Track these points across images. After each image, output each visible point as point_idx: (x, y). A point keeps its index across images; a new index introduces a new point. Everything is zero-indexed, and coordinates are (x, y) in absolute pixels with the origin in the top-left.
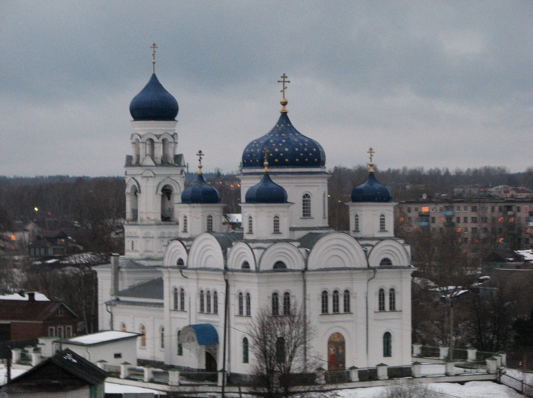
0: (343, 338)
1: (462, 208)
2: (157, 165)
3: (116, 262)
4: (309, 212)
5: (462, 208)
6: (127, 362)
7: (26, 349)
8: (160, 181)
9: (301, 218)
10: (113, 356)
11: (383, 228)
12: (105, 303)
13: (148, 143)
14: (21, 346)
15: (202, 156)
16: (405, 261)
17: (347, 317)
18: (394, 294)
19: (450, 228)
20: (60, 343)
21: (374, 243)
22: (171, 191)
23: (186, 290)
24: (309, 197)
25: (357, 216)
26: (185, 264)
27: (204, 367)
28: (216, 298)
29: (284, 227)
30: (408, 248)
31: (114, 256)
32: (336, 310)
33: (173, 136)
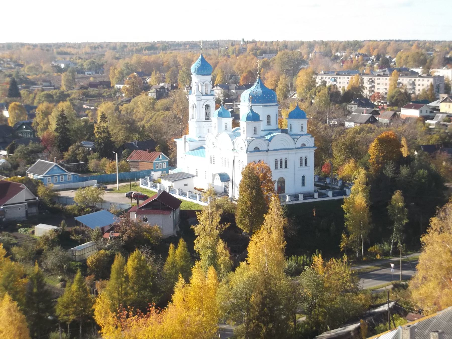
1: (338, 78)
2: (203, 95)
3: (185, 139)
4: (270, 123)
5: (338, 78)
8: (204, 102)
10: (188, 185)
14: (143, 177)
17: (286, 170)
18: (307, 159)
19: (330, 273)
21: (299, 137)
24: (270, 116)
29: (260, 133)
32: (281, 167)
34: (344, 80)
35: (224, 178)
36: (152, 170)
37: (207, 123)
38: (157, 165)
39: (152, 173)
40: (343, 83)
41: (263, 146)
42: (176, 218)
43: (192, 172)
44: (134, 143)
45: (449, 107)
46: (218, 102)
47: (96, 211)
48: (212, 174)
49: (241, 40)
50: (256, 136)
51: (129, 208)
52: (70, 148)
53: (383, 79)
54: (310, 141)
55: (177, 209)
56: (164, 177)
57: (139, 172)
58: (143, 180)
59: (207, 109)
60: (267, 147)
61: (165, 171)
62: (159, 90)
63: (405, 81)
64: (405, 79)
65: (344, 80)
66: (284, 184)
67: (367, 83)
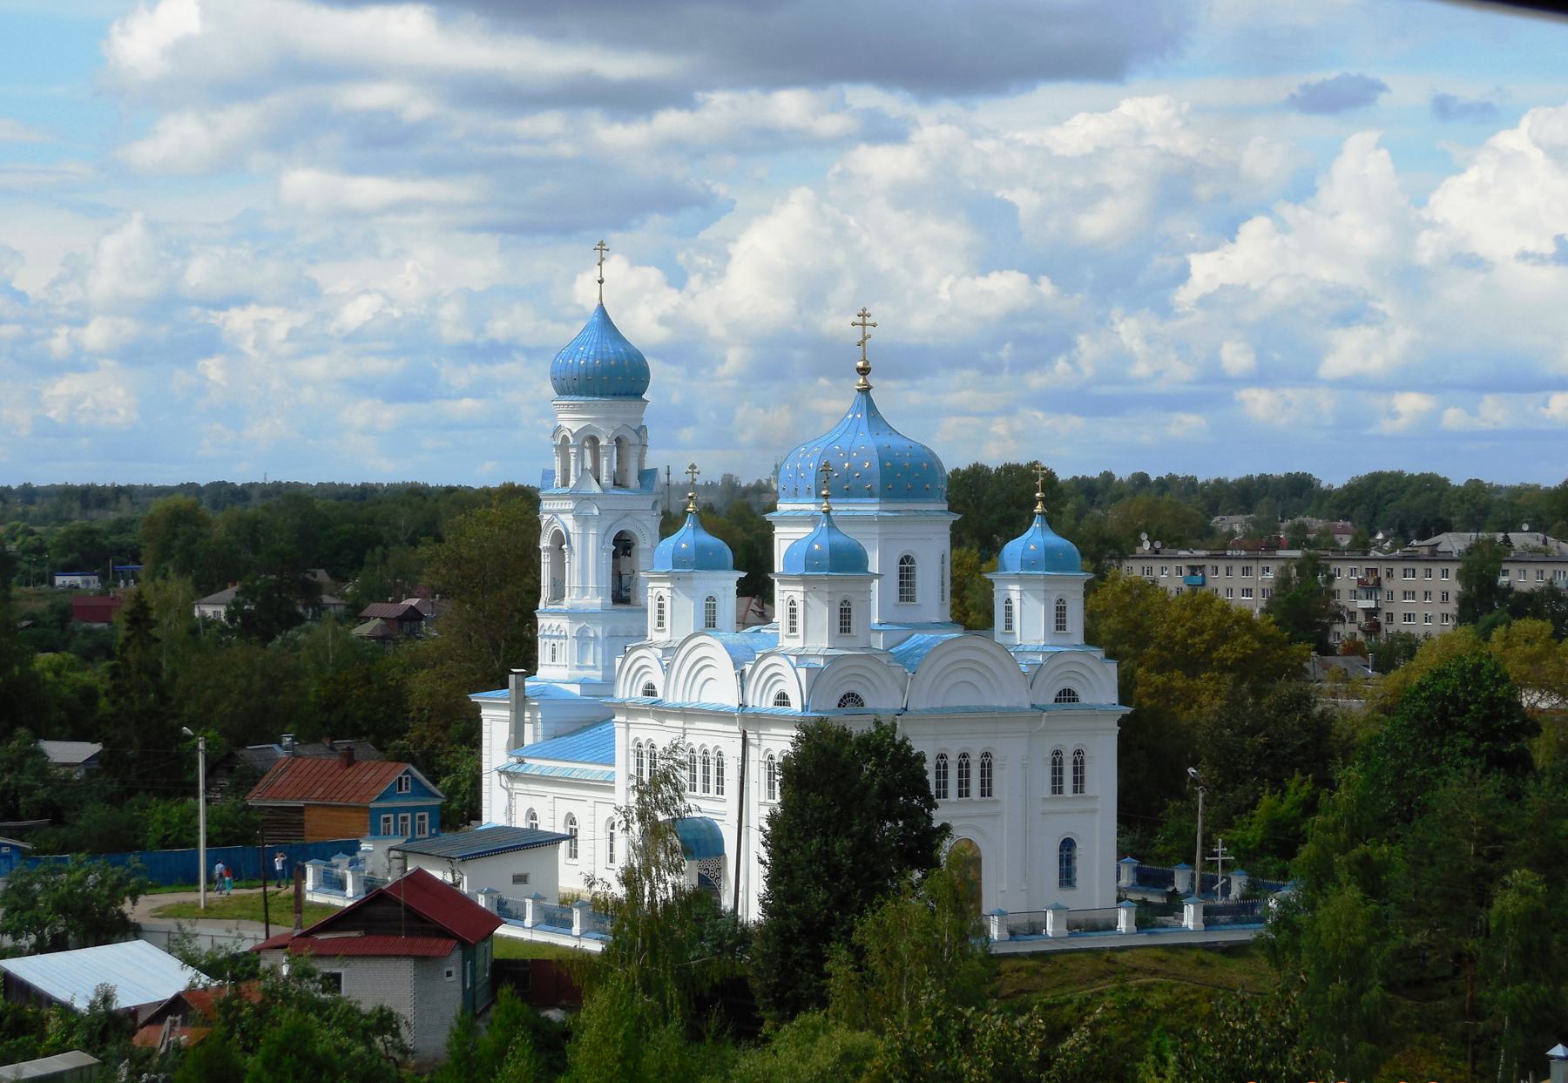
0: (977, 850)
1: (1222, 570)
4: (913, 592)
5: (1222, 570)
6: (1060, 903)
7: (334, 860)
8: (610, 522)
9: (895, 605)
10: (531, 879)
12: (496, 769)
13: (587, 444)
15: (696, 476)
20: (405, 853)
22: (633, 544)
24: (912, 562)
26: (660, 696)
28: (720, 764)
31: (516, 673)
33: (637, 432)
34: (1247, 581)
37: (623, 616)
38: (387, 820)
42: (473, 984)
53: (1429, 573)
59: (625, 554)
60: (900, 697)
65: (1247, 581)
66: (979, 871)
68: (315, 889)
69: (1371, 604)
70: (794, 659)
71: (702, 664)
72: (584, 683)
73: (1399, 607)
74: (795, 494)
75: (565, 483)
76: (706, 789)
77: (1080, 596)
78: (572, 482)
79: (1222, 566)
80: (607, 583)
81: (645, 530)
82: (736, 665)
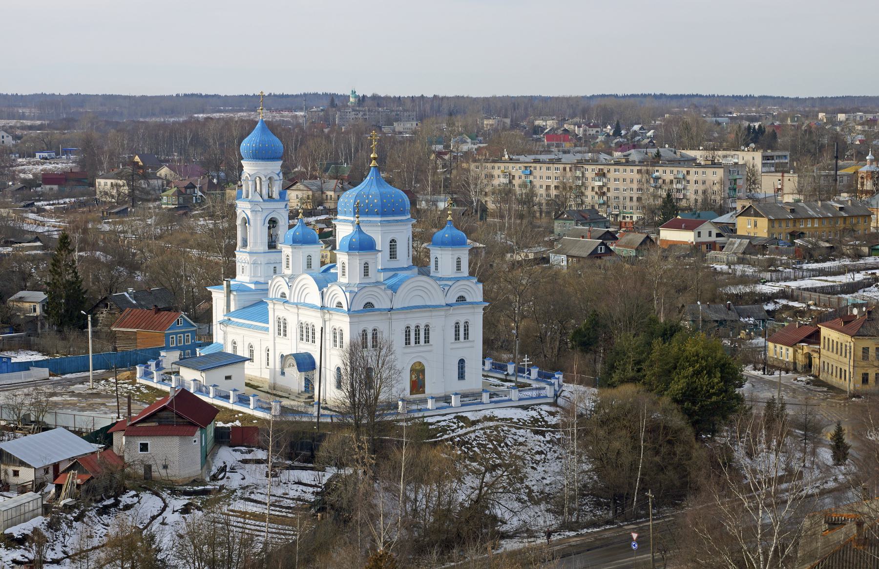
1: (538, 168)
3: (228, 286)
4: (396, 254)
5: (538, 168)
8: (266, 214)
10: (232, 378)
11: (459, 268)
14: (144, 362)
16: (480, 298)
17: (427, 348)
21: (450, 283)
23: (288, 321)
24: (395, 242)
25: (436, 258)
26: (288, 298)
27: (303, 389)
28: (313, 330)
30: (481, 286)
32: (417, 342)
34: (549, 173)
35: (305, 363)
36: (163, 349)
37: (273, 256)
38: (173, 338)
39: (163, 353)
40: (549, 178)
41: (382, 301)
42: (206, 443)
43: (242, 352)
44: (127, 295)
45: (755, 225)
46: (293, 215)
47: (44, 430)
48: (282, 356)
49: (349, 93)
50: (367, 281)
51: (113, 425)
52: (740, 286)
53: (625, 171)
54: (475, 291)
55: (209, 426)
56: (184, 361)
57: (136, 352)
58: (143, 368)
61: (190, 351)
62: (183, 190)
63: (666, 173)
64: (668, 169)
65: (549, 173)
67: (593, 179)
68: (141, 377)
69: (601, 184)
70: (344, 288)
71: (303, 288)
72: (256, 283)
73: (612, 185)
74: (345, 213)
75: (247, 197)
76: (308, 340)
77: (467, 256)
78: (250, 197)
79: (538, 166)
80: (266, 239)
81: (283, 221)
82: (320, 290)
